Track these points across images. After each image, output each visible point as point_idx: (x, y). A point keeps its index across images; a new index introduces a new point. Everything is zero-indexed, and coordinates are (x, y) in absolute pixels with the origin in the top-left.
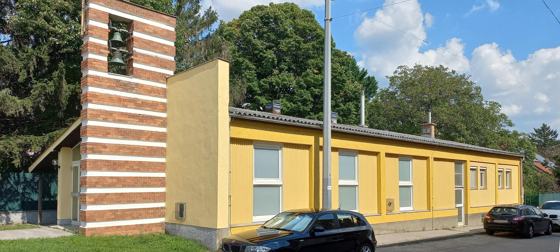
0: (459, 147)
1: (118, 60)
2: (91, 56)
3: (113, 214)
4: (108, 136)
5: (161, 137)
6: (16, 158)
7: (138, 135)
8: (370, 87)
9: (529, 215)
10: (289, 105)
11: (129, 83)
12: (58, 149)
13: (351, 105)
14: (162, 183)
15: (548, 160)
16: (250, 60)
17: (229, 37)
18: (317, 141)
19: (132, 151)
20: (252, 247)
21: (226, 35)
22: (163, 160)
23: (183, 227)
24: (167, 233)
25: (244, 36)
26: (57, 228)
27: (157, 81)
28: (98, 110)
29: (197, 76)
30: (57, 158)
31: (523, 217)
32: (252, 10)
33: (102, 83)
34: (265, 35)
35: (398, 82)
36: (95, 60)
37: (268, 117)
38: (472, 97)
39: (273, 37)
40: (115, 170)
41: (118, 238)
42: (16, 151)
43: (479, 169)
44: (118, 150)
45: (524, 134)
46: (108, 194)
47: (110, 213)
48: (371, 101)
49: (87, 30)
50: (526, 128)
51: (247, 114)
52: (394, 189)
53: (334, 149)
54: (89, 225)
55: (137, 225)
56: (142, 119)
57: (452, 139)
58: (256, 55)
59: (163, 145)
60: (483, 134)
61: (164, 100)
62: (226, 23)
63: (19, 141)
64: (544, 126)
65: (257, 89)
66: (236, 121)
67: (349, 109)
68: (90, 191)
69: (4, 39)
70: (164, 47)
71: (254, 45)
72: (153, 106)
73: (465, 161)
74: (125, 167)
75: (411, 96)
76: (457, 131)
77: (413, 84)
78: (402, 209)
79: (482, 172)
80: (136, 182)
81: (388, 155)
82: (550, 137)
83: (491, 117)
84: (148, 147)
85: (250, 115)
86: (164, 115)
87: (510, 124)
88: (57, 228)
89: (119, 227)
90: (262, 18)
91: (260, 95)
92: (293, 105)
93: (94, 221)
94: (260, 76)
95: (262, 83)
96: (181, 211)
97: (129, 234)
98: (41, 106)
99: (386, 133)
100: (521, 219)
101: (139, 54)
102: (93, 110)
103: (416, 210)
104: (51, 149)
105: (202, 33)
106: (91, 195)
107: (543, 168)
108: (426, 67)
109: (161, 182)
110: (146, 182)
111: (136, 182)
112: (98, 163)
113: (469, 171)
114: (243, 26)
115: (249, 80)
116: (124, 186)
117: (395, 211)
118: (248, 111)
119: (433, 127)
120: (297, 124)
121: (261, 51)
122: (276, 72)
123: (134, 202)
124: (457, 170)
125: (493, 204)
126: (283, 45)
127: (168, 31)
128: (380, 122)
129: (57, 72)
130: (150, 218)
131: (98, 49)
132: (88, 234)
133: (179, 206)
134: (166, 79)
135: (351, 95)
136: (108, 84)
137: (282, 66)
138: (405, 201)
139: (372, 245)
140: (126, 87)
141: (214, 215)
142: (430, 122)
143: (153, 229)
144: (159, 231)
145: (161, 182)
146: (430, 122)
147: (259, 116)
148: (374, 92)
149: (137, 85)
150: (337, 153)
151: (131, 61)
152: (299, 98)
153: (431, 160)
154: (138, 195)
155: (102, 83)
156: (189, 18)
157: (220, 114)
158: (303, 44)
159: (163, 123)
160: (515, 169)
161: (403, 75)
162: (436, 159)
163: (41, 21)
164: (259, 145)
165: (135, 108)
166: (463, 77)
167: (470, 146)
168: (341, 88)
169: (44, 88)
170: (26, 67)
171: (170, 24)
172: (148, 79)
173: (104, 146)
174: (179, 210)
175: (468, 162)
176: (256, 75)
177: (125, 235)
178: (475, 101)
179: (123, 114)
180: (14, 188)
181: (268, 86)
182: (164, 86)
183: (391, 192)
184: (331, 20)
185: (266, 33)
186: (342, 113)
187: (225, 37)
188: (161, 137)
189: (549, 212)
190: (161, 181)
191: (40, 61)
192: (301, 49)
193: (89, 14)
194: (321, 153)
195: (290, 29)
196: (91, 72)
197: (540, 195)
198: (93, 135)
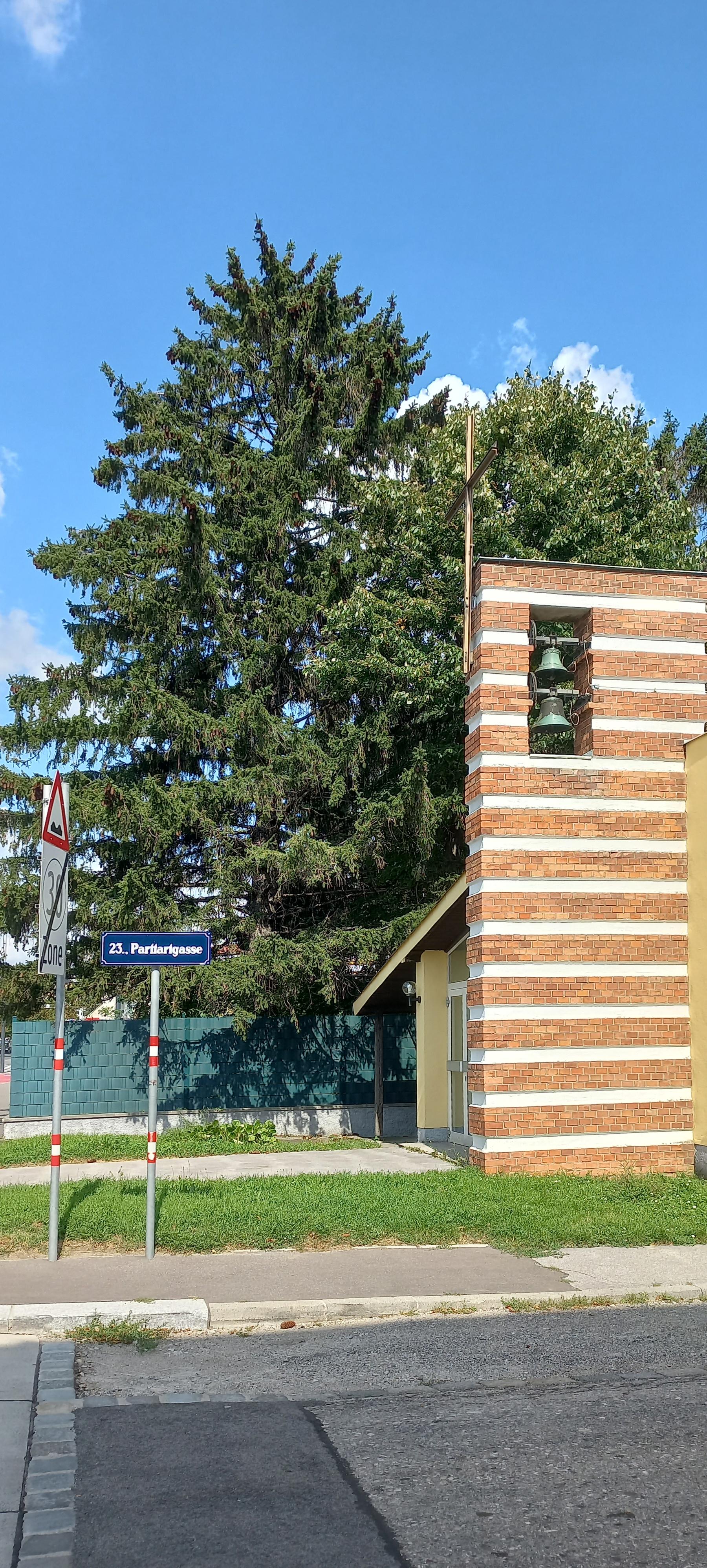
1: (554, 719)
2: (488, 720)
4: (533, 915)
6: (327, 981)
7: (608, 907)
11: (584, 773)
12: (415, 956)
14: (678, 1035)
19: (594, 949)
26: (418, 1150)
27: (659, 756)
28: (506, 852)
30: (412, 978)
33: (514, 784)
36: (498, 730)
40: (551, 1001)
41: (568, 1181)
44: (559, 949)
46: (537, 1065)
56: (618, 864)
63: (333, 942)
68: (491, 1057)
70: (677, 663)
72: (647, 825)
74: (579, 993)
84: (638, 937)
88: (418, 1150)
89: (570, 1152)
93: (504, 1134)
101: (608, 693)
102: (496, 854)
104: (400, 957)
106: (497, 1069)
116: (576, 1044)
129: (410, 773)
131: (504, 699)
132: (491, 1168)
140: (575, 785)
149: (603, 774)
155: (514, 784)
163: (373, 659)
165: (603, 837)
170: (344, 769)
171: (688, 594)
172: (633, 755)
173: (524, 942)
179: (568, 856)
180: (325, 1053)
182: (678, 767)
188: (672, 908)
191: (373, 750)
193: (483, 616)
198: (499, 916)
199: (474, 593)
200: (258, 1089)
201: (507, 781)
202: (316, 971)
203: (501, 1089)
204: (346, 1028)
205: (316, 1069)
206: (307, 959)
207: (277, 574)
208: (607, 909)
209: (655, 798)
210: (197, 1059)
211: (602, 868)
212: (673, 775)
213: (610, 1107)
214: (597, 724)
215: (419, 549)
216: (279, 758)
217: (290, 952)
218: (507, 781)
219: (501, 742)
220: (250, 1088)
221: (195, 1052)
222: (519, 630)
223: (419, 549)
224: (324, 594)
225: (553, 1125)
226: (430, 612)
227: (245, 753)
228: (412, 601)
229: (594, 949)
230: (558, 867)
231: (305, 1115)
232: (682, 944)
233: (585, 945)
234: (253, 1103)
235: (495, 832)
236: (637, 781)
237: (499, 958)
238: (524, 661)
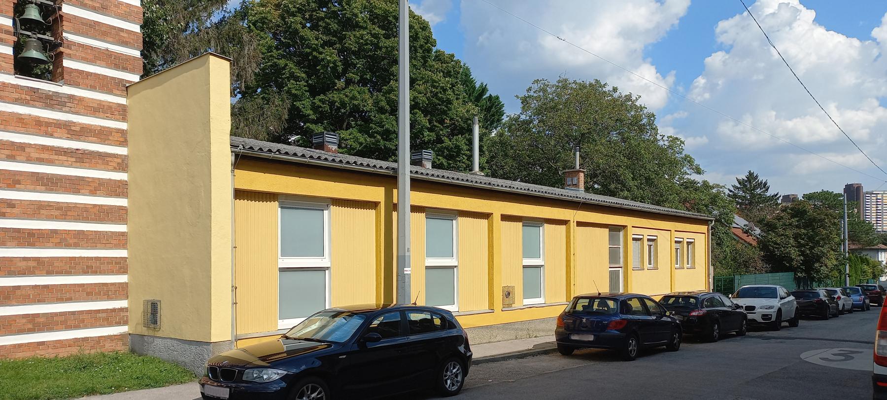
1: (34, 54)
4: (17, 186)
5: (118, 189)
7: (74, 185)
9: (713, 306)
10: (362, 140)
13: (461, 140)
14: (121, 268)
15: (752, 224)
16: (298, 64)
17: (261, 24)
18: (389, 196)
20: (256, 371)
21: (257, 21)
22: (122, 228)
24: (133, 351)
25: (286, 23)
27: (110, 92)
29: (175, 82)
31: (705, 310)
34: (320, 23)
35: (534, 104)
37: (303, 156)
38: (642, 129)
39: (334, 26)
40: (32, 245)
41: (38, 362)
44: (37, 210)
45: (718, 186)
46: (18, 287)
47: (24, 321)
48: (493, 135)
50: (723, 178)
51: (300, 155)
53: (415, 209)
57: (613, 194)
59: (122, 202)
60: (656, 187)
61: (123, 126)
64: (751, 174)
65: (310, 112)
66: (244, 160)
67: (457, 147)
70: (122, 34)
72: (102, 135)
73: (625, 227)
76: (618, 181)
77: (554, 108)
78: (527, 302)
79: (651, 243)
81: (505, 218)
82: (758, 191)
83: (669, 159)
84: (95, 205)
86: (122, 151)
87: (699, 171)
89: (42, 343)
91: (315, 122)
94: (314, 91)
96: (153, 312)
97: (61, 355)
99: (518, 186)
100: (701, 313)
101: (74, 44)
103: (548, 302)
107: (744, 236)
109: (119, 266)
115: (295, 98)
116: (49, 273)
117: (516, 305)
118: (300, 150)
119: (582, 175)
120: (354, 167)
121: (314, 50)
123: (69, 300)
124: (613, 240)
125: (667, 292)
126: (351, 40)
128: (507, 168)
130: (101, 326)
133: (149, 306)
134: (126, 88)
136: (16, 96)
138: (532, 289)
139: (465, 361)
141: (207, 322)
142: (578, 167)
145: (119, 266)
146: (578, 167)
147: (287, 153)
148: (499, 120)
149: (71, 97)
151: (60, 55)
152: (379, 129)
153: (573, 225)
154: (77, 289)
157: (213, 149)
159: (122, 164)
160: (699, 238)
161: (541, 94)
162: (580, 224)
164: (288, 201)
165: (68, 139)
166: (628, 98)
167: (638, 204)
168: (445, 113)
172: (93, 88)
174: (150, 310)
175: (629, 228)
176: (307, 88)
177: (52, 356)
178: (646, 137)
179: (44, 148)
181: (327, 108)
182: (122, 101)
183: (510, 275)
185: (322, 19)
187: (254, 24)
188: (118, 189)
189: (744, 302)
190: (119, 263)
192: (381, 49)
194: (395, 214)
195: (363, 16)
197: (736, 277)
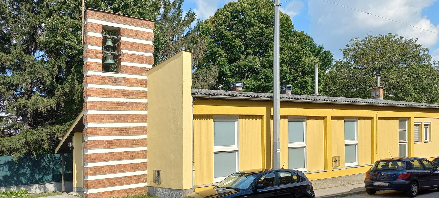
0: (434, 107)
1: (110, 61)
2: (89, 60)
3: (107, 182)
4: (103, 121)
5: (143, 119)
6: (45, 143)
7: (125, 119)
8: (326, 60)
10: (254, 83)
12: (72, 134)
13: (308, 78)
14: (144, 155)
16: (223, 49)
17: (206, 32)
18: (268, 111)
19: (121, 131)
21: (204, 31)
22: (144, 137)
23: (160, 189)
26: (71, 194)
27: (140, 74)
28: (95, 102)
29: (168, 65)
30: (71, 142)
32: (225, 7)
33: (98, 80)
34: (234, 27)
35: (351, 53)
36: (92, 63)
37: (225, 95)
38: (420, 59)
39: (240, 27)
40: (108, 147)
42: (46, 138)
43: (423, 124)
44: (110, 131)
46: (103, 166)
47: (106, 181)
48: (327, 72)
49: (86, 40)
52: (337, 148)
53: (282, 117)
54: (91, 191)
55: (126, 190)
56: (128, 106)
58: (226, 45)
59: (145, 125)
61: (145, 89)
62: (204, 21)
63: (48, 130)
65: (228, 72)
66: (198, 100)
68: (90, 165)
69: (39, 55)
70: (145, 47)
71: (225, 36)
72: (137, 94)
73: (409, 118)
74: (117, 144)
75: (363, 64)
78: (347, 165)
80: (125, 156)
81: (334, 118)
85: (210, 94)
86: (145, 101)
88: (71, 194)
89: (113, 191)
90: (231, 13)
91: (231, 77)
92: (258, 83)
93: (94, 188)
94: (230, 61)
95: (233, 67)
96: (158, 176)
98: (61, 102)
99: (342, 100)
101: (125, 54)
102: (92, 102)
103: (360, 165)
104: (67, 135)
105: (183, 32)
106: (91, 168)
108: (376, 37)
110: (131, 156)
111: (125, 156)
112: (96, 143)
113: (413, 127)
114: (217, 21)
115: (221, 66)
116: (115, 160)
117: (341, 167)
118: (223, 92)
119: (381, 90)
121: (231, 41)
122: (243, 56)
124: (401, 126)
127: (148, 33)
129: (71, 76)
130: (136, 183)
131: (94, 54)
134: (146, 71)
135: (308, 69)
137: (248, 51)
138: (350, 157)
140: (116, 81)
142: (379, 85)
143: (138, 192)
144: (143, 193)
146: (379, 85)
147: (217, 94)
148: (330, 64)
149: (124, 79)
150: (287, 120)
152: (263, 76)
153: (376, 119)
155: (98, 80)
156: (174, 21)
158: (265, 29)
161: (356, 46)
163: (59, 38)
164: (218, 118)
165: (123, 98)
166: (411, 41)
168: (298, 64)
169: (63, 89)
170: (51, 74)
171: (148, 26)
172: (133, 73)
173: (100, 129)
176: (227, 61)
182: (145, 78)
183: (337, 150)
184: (280, 5)
185: (235, 24)
186: (299, 85)
187: (203, 33)
188: (143, 119)
191: (60, 68)
192: (264, 35)
193: (88, 27)
194: (271, 121)
196: (90, 73)
198: (92, 122)
199: (85, 20)
200: (25, 178)
201: (96, 80)
202: (42, 140)
203: (93, 174)
204: (55, 157)
205: (45, 170)
206: (39, 136)
207: (28, 7)
208: (125, 119)
209: (139, 86)
210: (3, 170)
211: (124, 107)
212: (144, 80)
213: (125, 177)
214: (123, 63)
215: (74, 4)
216: (30, 69)
217: (33, 134)
218: (96, 80)
219: (93, 67)
220: (23, 178)
221: (2, 168)
222: (99, 33)
223: (74, 4)
224: (44, 15)
225: (108, 184)
226: (77, 24)
227: (17, 67)
228: (71, 20)
229: (121, 131)
230: (111, 107)
231: (42, 185)
232: (145, 129)
233: (119, 130)
234: (24, 182)
235: (92, 95)
236: (134, 81)
237: (93, 134)
238: (101, 42)
